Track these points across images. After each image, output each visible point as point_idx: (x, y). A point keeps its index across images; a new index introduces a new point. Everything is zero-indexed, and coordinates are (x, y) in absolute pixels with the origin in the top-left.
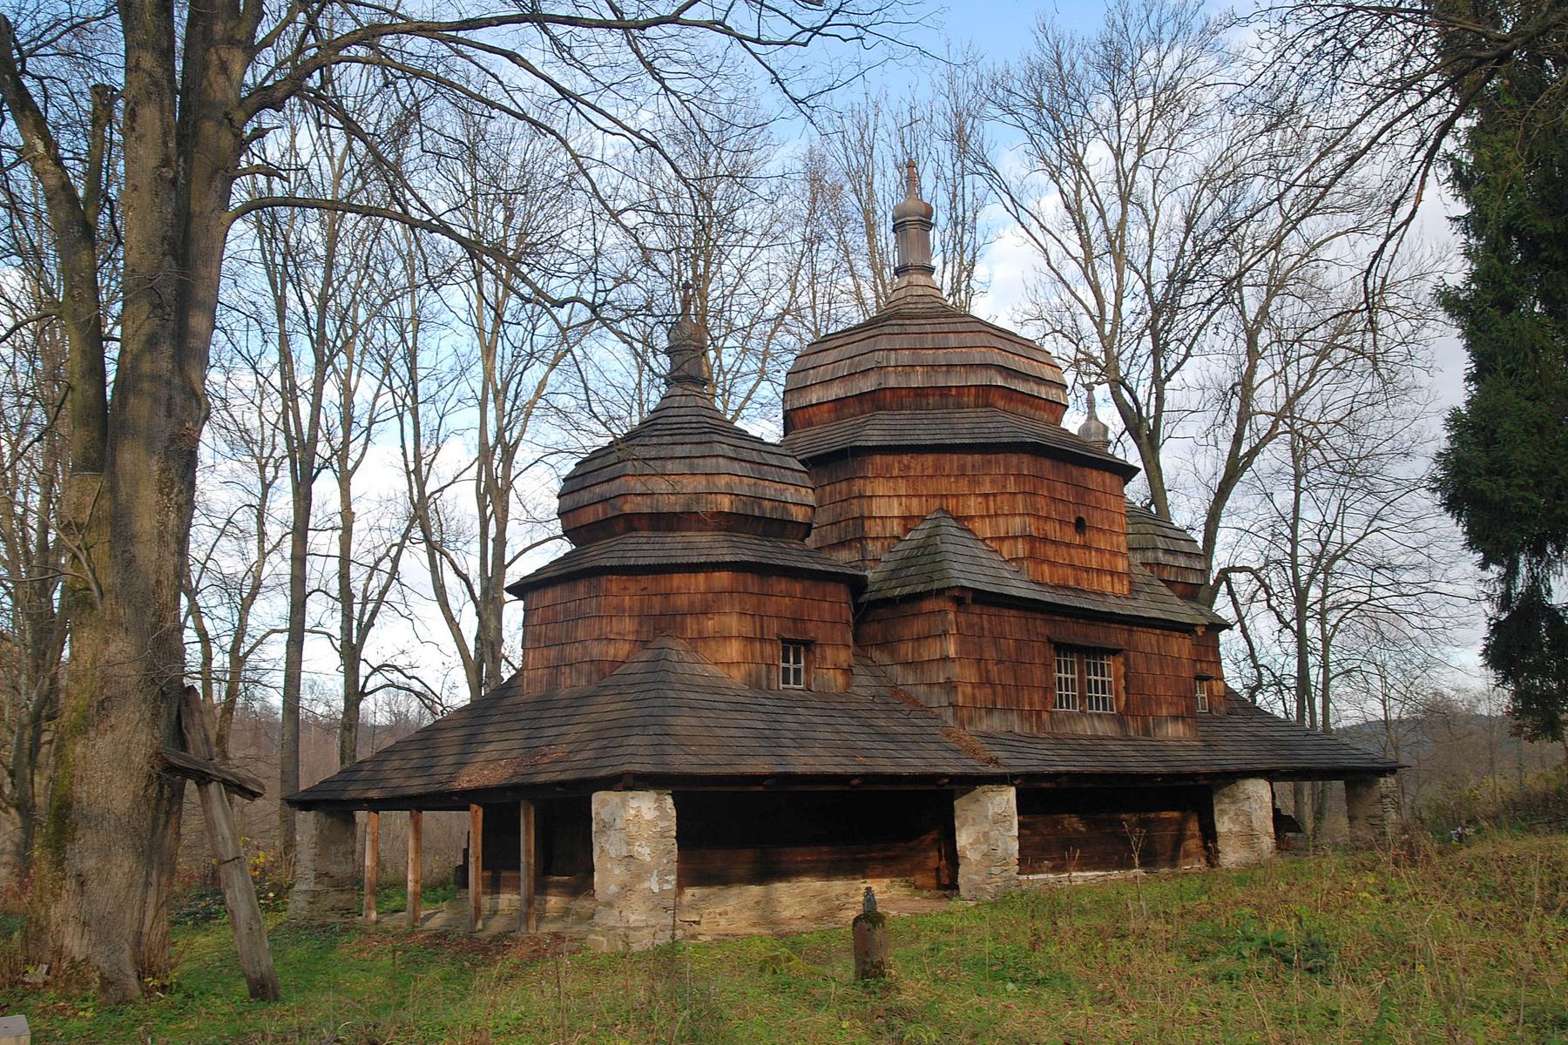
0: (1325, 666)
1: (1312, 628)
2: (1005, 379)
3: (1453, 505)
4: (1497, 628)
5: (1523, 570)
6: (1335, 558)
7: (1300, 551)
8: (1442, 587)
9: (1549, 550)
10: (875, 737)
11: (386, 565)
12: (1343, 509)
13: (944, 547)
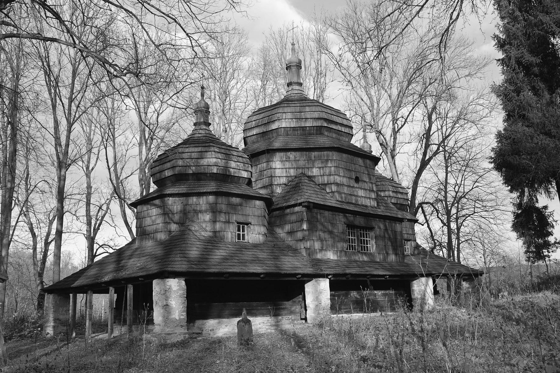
0: (458, 238)
1: (453, 226)
2: (328, 124)
3: (498, 168)
4: (517, 216)
5: (526, 194)
6: (461, 198)
7: (448, 195)
8: (502, 208)
9: (536, 186)
12: (464, 179)
13: (302, 187)
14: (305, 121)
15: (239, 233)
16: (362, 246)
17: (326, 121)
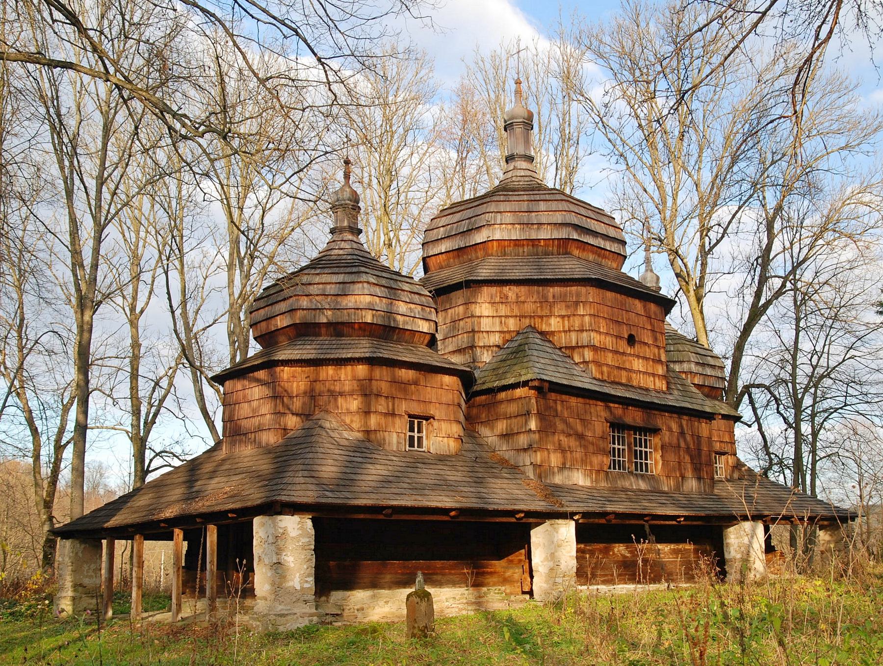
0: (813, 452)
2: (579, 235)
6: (822, 377)
10: (473, 485)
11: (164, 383)
12: (828, 342)
14: (538, 228)
15: (420, 435)
16: (636, 463)
17: (576, 230)
